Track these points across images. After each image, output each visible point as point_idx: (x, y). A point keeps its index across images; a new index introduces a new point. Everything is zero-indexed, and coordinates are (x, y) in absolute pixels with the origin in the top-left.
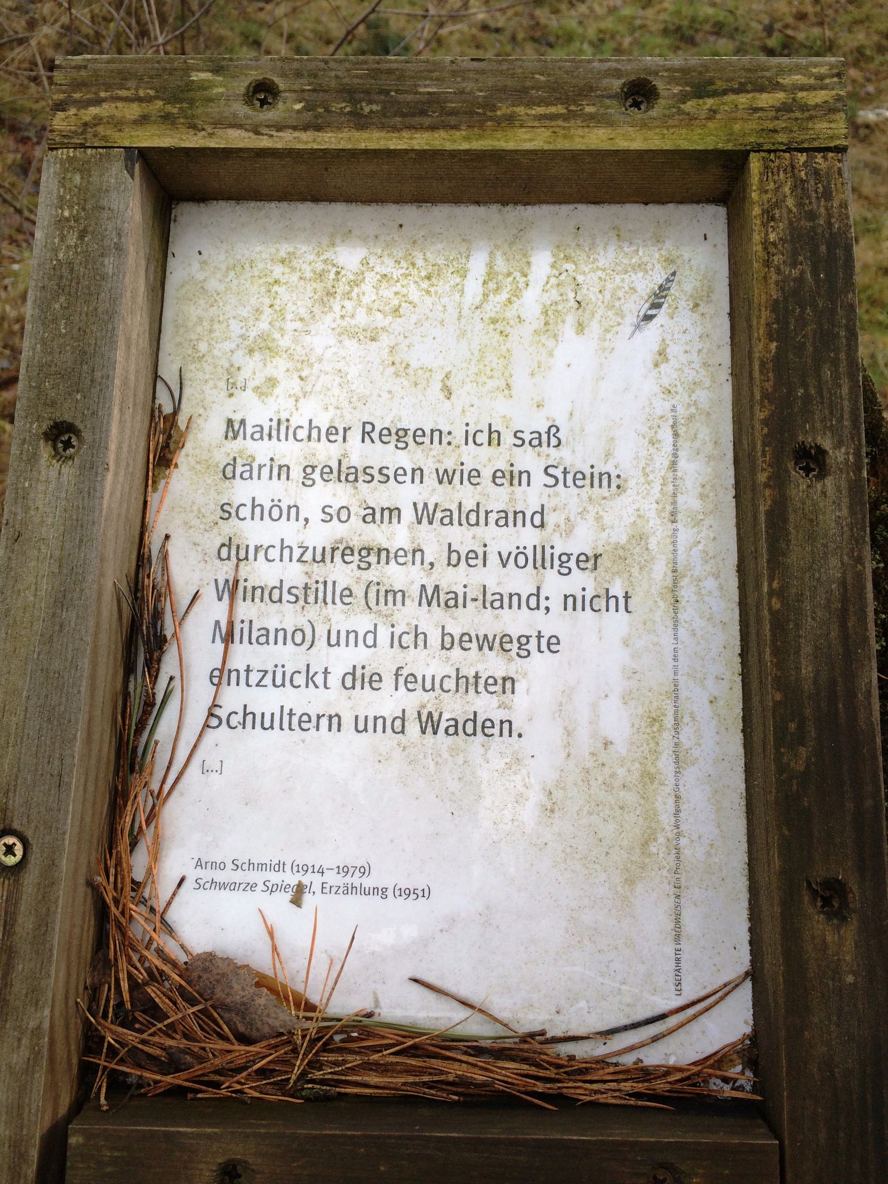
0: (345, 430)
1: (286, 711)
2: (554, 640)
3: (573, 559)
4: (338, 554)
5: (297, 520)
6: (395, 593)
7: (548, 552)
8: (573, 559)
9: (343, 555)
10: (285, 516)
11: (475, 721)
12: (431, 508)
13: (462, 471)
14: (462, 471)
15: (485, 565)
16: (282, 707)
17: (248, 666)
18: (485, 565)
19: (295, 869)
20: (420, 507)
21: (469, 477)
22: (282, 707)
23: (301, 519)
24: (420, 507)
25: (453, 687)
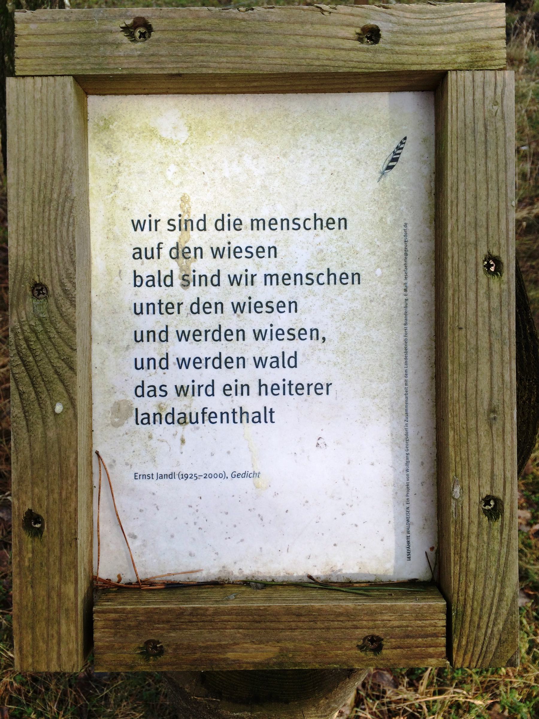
0: (328, 385)
1: (268, 410)
4: (312, 389)
5: (318, 339)
6: (271, 276)
9: (316, 389)
11: (220, 331)
13: (229, 248)
14: (229, 248)
15: (328, 394)
16: (265, 408)
17: (160, 301)
18: (328, 394)
20: (257, 332)
21: (277, 334)
22: (265, 408)
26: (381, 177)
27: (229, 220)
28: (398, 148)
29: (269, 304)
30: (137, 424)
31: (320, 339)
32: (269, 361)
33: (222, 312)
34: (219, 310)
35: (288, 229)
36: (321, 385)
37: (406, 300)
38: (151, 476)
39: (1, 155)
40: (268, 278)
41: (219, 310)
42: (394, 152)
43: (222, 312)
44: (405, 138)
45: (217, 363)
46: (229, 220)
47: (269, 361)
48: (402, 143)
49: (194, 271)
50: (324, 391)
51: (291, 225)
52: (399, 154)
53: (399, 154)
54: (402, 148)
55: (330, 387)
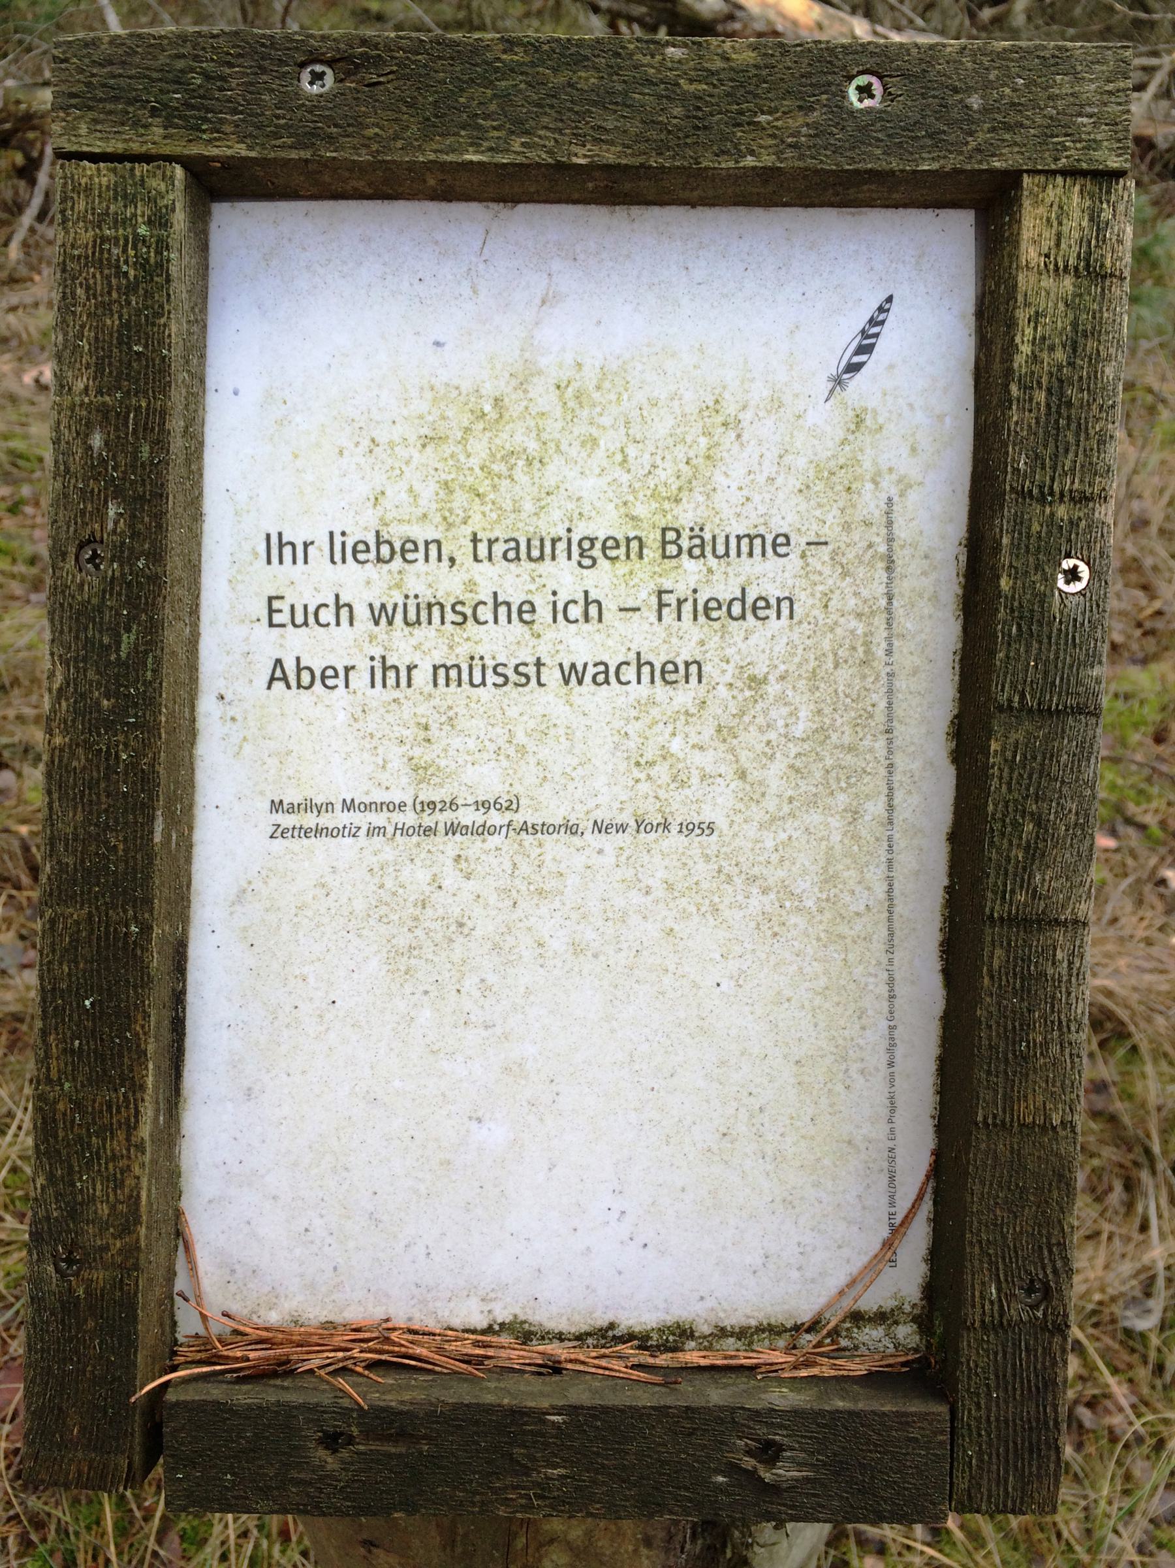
0: (347, 670)
2: (781, 540)
3: (598, 545)
5: (440, 559)
7: (338, 540)
8: (598, 545)
10: (311, 610)
12: (580, 668)
19: (419, 808)
20: (377, 606)
23: (445, 557)
24: (377, 606)
25: (490, 617)
26: (832, 391)
27: (343, 544)
28: (873, 322)
29: (523, 680)
30: (333, 562)
31: (446, 562)
32: (591, 671)
33: (306, 562)
34: (785, 611)
35: (443, 623)
36: (615, 539)
37: (891, 1150)
38: (531, 670)
39: (23, 631)
40: (442, 672)
41: (785, 611)
42: (863, 331)
43: (306, 562)
44: (890, 299)
45: (736, 609)
46: (343, 544)
47: (591, 671)
48: (881, 309)
49: (343, 534)
50: (340, 682)
51: (450, 616)
52: (877, 335)
53: (877, 335)
54: (882, 323)
55: (351, 673)
